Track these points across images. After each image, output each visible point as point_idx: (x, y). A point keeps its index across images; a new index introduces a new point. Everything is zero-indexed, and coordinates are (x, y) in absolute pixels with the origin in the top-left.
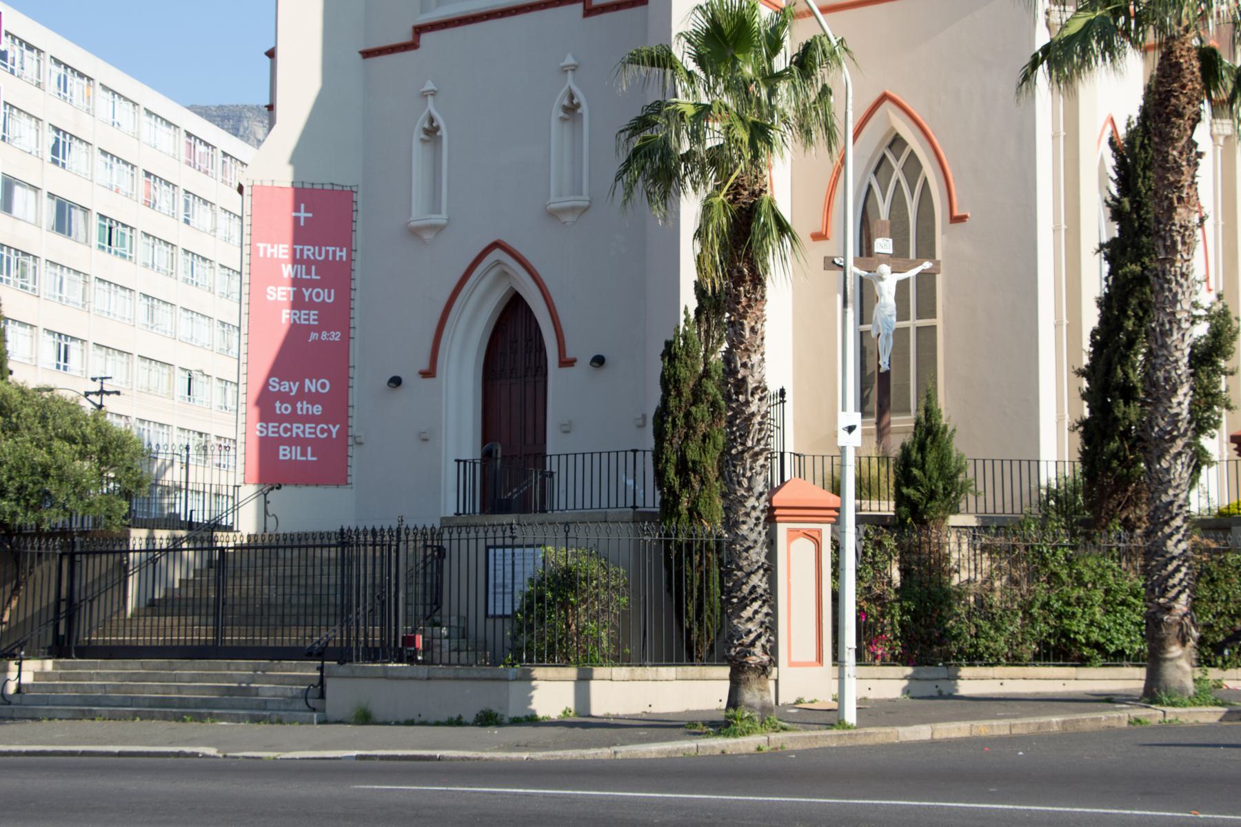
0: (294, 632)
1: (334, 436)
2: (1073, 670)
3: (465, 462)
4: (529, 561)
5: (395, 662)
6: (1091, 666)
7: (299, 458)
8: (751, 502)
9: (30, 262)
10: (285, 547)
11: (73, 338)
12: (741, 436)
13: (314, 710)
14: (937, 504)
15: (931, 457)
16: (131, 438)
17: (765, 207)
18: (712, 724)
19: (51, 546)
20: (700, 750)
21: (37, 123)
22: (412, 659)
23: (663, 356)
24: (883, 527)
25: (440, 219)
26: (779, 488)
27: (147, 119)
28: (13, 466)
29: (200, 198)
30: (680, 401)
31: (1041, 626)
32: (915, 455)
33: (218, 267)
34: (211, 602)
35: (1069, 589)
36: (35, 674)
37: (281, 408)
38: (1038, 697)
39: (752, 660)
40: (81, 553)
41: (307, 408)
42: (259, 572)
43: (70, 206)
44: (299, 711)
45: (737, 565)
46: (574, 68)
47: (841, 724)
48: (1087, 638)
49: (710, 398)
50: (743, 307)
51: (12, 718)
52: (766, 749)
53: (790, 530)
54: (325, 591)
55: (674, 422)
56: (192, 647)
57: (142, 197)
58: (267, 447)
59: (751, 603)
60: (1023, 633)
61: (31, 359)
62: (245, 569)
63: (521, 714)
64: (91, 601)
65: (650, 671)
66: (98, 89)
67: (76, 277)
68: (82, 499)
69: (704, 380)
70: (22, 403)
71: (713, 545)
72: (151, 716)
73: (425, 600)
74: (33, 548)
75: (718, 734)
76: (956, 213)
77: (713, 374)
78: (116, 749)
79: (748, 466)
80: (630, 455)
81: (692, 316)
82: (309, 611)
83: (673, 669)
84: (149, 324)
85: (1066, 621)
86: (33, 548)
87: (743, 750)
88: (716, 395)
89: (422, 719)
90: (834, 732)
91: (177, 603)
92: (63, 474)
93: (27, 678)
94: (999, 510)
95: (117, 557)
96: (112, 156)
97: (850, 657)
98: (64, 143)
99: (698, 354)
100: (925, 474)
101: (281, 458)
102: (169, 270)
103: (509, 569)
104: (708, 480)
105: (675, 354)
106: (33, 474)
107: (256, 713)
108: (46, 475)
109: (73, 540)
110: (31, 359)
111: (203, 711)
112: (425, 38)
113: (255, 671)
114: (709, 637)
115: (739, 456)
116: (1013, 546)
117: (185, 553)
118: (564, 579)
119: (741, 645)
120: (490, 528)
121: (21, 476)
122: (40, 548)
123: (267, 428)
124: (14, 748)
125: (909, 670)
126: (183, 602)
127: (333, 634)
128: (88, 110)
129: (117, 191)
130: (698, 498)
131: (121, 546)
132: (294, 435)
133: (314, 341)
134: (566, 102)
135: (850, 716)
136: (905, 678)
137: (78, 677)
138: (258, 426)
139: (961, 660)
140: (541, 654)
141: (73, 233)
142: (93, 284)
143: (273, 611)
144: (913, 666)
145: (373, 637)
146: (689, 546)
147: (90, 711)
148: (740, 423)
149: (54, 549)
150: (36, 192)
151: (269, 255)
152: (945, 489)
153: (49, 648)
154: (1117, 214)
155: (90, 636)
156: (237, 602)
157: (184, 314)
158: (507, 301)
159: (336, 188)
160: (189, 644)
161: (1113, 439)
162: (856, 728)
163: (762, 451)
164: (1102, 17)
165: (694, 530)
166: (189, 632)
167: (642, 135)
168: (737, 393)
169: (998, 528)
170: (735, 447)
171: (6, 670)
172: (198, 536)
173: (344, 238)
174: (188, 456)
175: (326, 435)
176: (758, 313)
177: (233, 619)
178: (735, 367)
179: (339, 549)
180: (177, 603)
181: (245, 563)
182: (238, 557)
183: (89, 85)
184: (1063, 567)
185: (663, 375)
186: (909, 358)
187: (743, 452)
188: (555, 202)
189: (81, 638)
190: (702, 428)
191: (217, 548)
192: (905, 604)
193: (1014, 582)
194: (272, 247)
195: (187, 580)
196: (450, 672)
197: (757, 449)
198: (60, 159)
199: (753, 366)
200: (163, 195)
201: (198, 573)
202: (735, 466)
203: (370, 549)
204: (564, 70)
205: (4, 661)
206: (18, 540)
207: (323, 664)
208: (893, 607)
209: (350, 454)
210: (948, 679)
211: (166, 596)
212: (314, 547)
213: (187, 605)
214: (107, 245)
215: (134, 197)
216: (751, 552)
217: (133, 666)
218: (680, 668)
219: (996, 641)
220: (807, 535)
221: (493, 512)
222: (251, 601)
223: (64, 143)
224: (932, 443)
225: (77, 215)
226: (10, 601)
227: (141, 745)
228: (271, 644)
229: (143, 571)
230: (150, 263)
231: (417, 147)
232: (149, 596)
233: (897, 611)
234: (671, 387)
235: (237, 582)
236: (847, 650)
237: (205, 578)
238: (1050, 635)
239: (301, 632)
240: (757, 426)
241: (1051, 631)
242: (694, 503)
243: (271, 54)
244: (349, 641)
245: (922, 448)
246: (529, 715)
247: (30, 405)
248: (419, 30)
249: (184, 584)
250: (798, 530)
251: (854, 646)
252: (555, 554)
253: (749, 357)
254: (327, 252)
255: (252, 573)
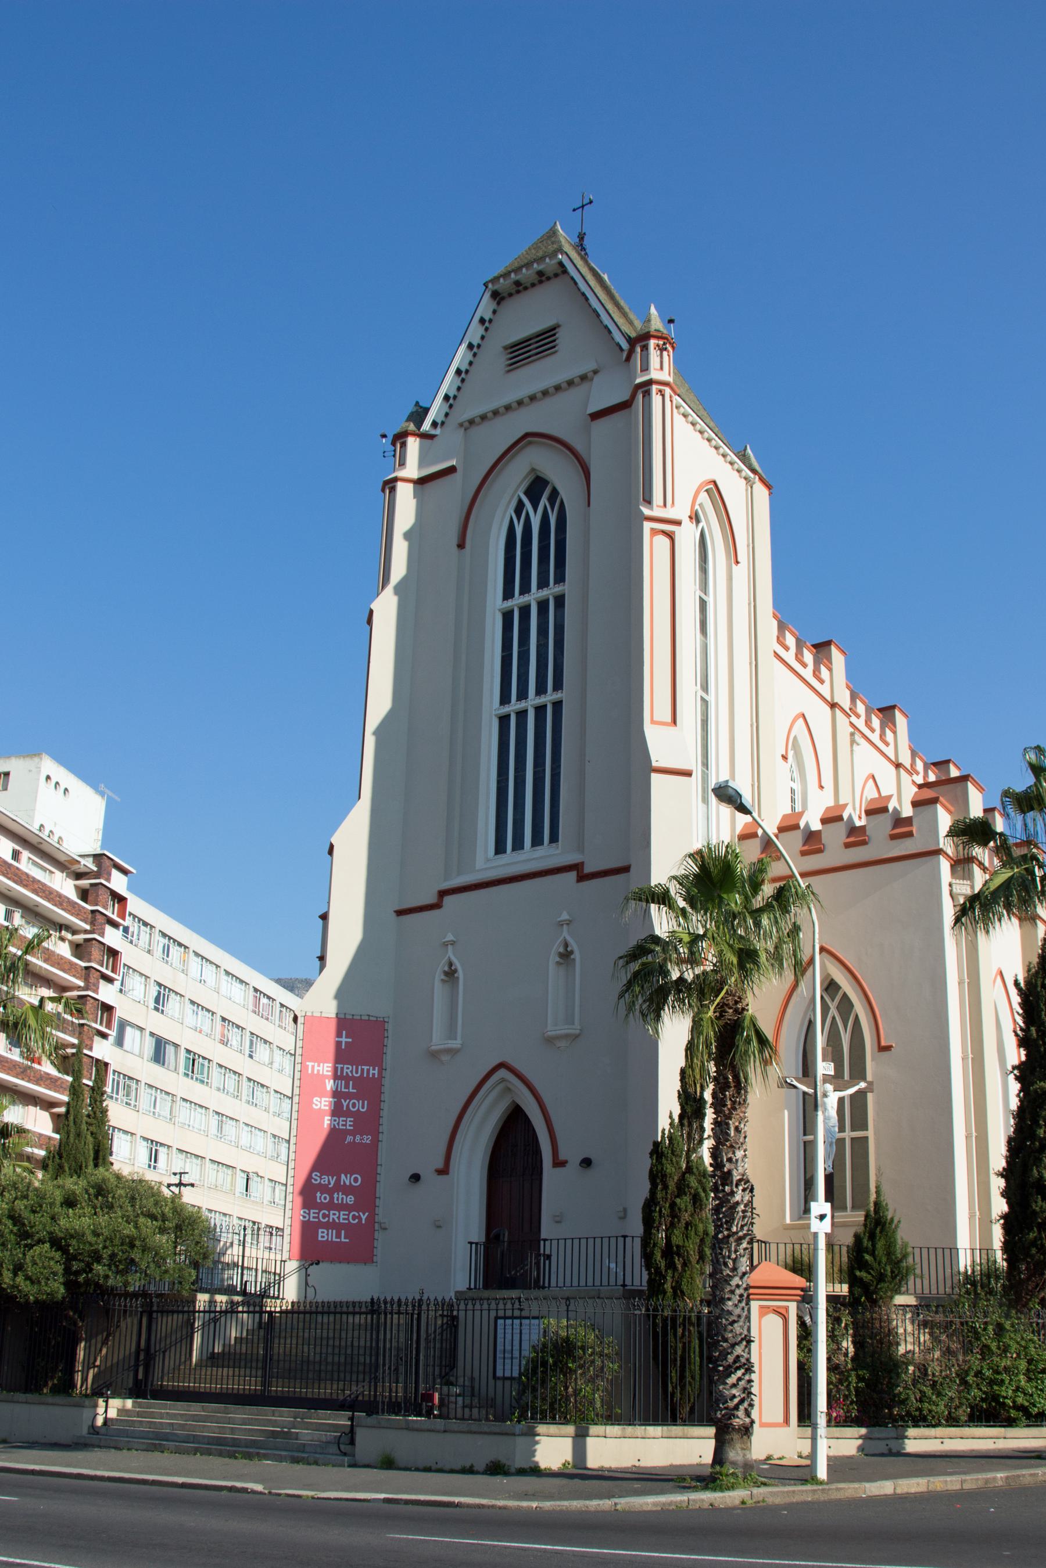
0: (329, 1386)
1: (363, 1222)
2: (1002, 1430)
3: (477, 1244)
4: (534, 1331)
5: (415, 1416)
6: (1017, 1426)
7: (334, 1239)
8: (736, 1281)
9: (134, 1085)
10: (323, 1313)
11: (162, 1145)
12: (727, 1222)
13: (345, 1454)
14: (886, 1285)
15: (880, 1244)
16: (200, 1218)
17: (747, 1022)
18: (699, 1478)
19: (134, 1305)
20: (691, 1503)
21: (146, 980)
22: (429, 1413)
23: (651, 1154)
24: (841, 1305)
25: (455, 1044)
26: (757, 1266)
27: (226, 978)
28: (107, 1238)
29: (261, 1038)
30: (666, 1193)
31: (975, 1392)
32: (866, 1243)
33: (272, 1092)
34: (261, 1357)
35: (998, 1360)
36: (119, 1410)
37: (321, 1198)
38: (974, 1454)
39: (736, 1422)
40: (157, 1312)
41: (342, 1198)
42: (301, 1334)
43: (166, 1043)
44: (332, 1454)
45: (723, 1337)
46: (569, 923)
47: (814, 1479)
48: (1014, 1402)
49: (693, 1191)
50: (729, 1109)
51: (100, 1447)
52: (750, 1502)
53: (761, 1307)
54: (355, 1352)
55: (660, 1211)
56: (244, 1395)
57: (218, 1037)
58: (308, 1230)
59: (736, 1371)
60: (959, 1398)
61: (130, 1159)
62: (289, 1330)
63: (525, 1466)
64: (164, 1352)
65: (640, 1430)
66: (192, 954)
67: (166, 1097)
68: (160, 1267)
69: (687, 1175)
70: (117, 1186)
71: (694, 1319)
72: (209, 1453)
73: (441, 1362)
74: (120, 1305)
75: (706, 1488)
76: (883, 1044)
77: (695, 1170)
78: (180, 1480)
79: (733, 1249)
80: (621, 1240)
81: (677, 1120)
82: (342, 1368)
83: (659, 1428)
84: (219, 1135)
85: (996, 1387)
86: (120, 1305)
87: (730, 1503)
88: (697, 1189)
89: (439, 1466)
90: (809, 1487)
91: (232, 1357)
92: (146, 1244)
93: (112, 1413)
94: (934, 1291)
95: (186, 1316)
96: (199, 1005)
97: (822, 1420)
98: (164, 995)
99: (682, 1153)
100: (875, 1259)
101: (320, 1239)
102: (236, 1093)
103: (517, 1337)
104: (690, 1262)
105: (662, 1153)
106: (122, 1244)
107: (296, 1454)
108: (132, 1246)
109: (151, 1300)
110: (130, 1159)
111: (251, 1450)
112: (448, 900)
113: (295, 1418)
114: (689, 1400)
115: (725, 1240)
116: (951, 1322)
117: (240, 1315)
118: (563, 1347)
119: (725, 1408)
120: (501, 1302)
121: (113, 1246)
122: (125, 1306)
123: (309, 1214)
124: (99, 1473)
125: (863, 1431)
126: (237, 1357)
127: (362, 1389)
128: (183, 970)
129: (200, 1032)
130: (681, 1276)
131: (189, 1307)
132: (331, 1220)
133: (349, 1143)
134: (561, 950)
135: (822, 1473)
136: (860, 1437)
137: (152, 1415)
138: (302, 1212)
139: (907, 1422)
140: (543, 1414)
141: (166, 1063)
142: (178, 1103)
143: (311, 1367)
144: (866, 1427)
145: (397, 1392)
146: (674, 1319)
147: (160, 1444)
148: (725, 1211)
149: (136, 1307)
150: (141, 1032)
151: (316, 1072)
152: (892, 1272)
153: (130, 1389)
154: (1023, 1042)
155: (162, 1382)
156: (281, 1358)
157: (246, 1128)
158: (509, 1112)
159: (371, 1018)
160: (241, 1392)
161: (1031, 1229)
162: (827, 1484)
163: (745, 1236)
164: (1019, 872)
165: (678, 1306)
166: (242, 1382)
167: (640, 961)
168: (723, 1185)
169: (937, 1307)
170: (722, 1232)
171: (96, 1406)
172: (252, 1302)
173: (377, 1059)
174: (245, 1235)
175: (357, 1220)
176: (742, 1115)
177: (278, 1372)
178: (722, 1161)
179: (369, 1316)
180: (232, 1357)
181: (289, 1326)
182: (283, 1321)
183: (185, 952)
184: (993, 1339)
185: (651, 1171)
186: (845, 1160)
187: (729, 1236)
188: (552, 1031)
189: (155, 1383)
190: (686, 1216)
191: (266, 1312)
192: (860, 1373)
193: (948, 1352)
194: (319, 1066)
195: (241, 1338)
196: (464, 1426)
197: (741, 1234)
198: (161, 1007)
199: (737, 1160)
200: (234, 1036)
201: (250, 1333)
202: (721, 1249)
203: (395, 1316)
204: (561, 924)
205: (95, 1398)
206: (109, 1298)
207: (353, 1415)
208: (850, 1376)
209: (376, 1237)
210: (897, 1438)
211: (224, 1350)
212: (348, 1313)
213: (240, 1359)
214: (190, 1073)
215: (213, 1037)
216: (736, 1325)
217: (196, 1409)
218: (665, 1428)
219: (938, 1405)
220: (776, 1311)
221: (500, 1287)
222: (293, 1358)
223: (164, 995)
224: (881, 1232)
225: (170, 1050)
226: (101, 1350)
227: (200, 1478)
228: (309, 1396)
229: (206, 1329)
230: (222, 1087)
231: (438, 984)
232: (210, 1350)
233: (853, 1379)
234: (658, 1181)
235: (282, 1341)
236: (819, 1413)
237: (256, 1337)
238: (983, 1400)
239: (335, 1387)
240: (741, 1214)
241: (984, 1396)
242: (677, 1282)
243: (324, 917)
244: (375, 1395)
245: (872, 1237)
246: (533, 1466)
247: (123, 1188)
248: (443, 894)
249: (238, 1341)
250: (768, 1307)
251: (825, 1410)
252: (558, 1325)
253: (734, 1153)
254: (363, 1070)
255: (294, 1334)
